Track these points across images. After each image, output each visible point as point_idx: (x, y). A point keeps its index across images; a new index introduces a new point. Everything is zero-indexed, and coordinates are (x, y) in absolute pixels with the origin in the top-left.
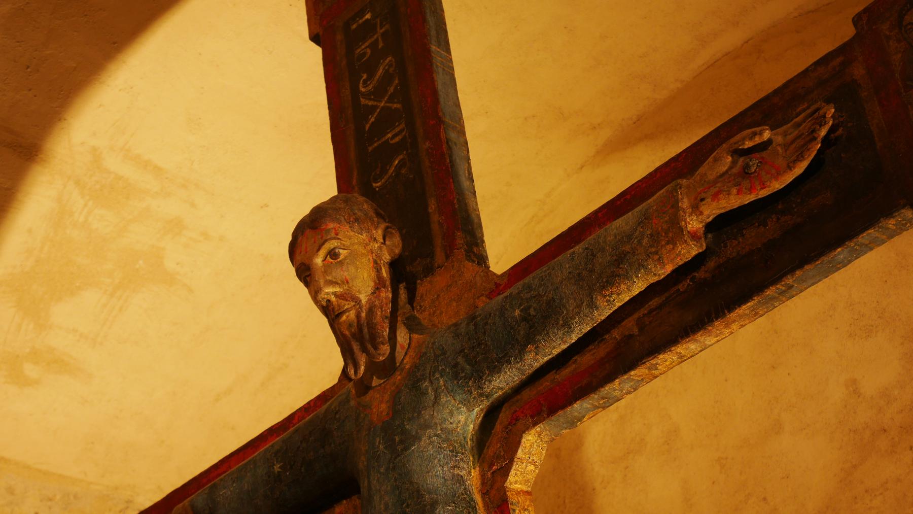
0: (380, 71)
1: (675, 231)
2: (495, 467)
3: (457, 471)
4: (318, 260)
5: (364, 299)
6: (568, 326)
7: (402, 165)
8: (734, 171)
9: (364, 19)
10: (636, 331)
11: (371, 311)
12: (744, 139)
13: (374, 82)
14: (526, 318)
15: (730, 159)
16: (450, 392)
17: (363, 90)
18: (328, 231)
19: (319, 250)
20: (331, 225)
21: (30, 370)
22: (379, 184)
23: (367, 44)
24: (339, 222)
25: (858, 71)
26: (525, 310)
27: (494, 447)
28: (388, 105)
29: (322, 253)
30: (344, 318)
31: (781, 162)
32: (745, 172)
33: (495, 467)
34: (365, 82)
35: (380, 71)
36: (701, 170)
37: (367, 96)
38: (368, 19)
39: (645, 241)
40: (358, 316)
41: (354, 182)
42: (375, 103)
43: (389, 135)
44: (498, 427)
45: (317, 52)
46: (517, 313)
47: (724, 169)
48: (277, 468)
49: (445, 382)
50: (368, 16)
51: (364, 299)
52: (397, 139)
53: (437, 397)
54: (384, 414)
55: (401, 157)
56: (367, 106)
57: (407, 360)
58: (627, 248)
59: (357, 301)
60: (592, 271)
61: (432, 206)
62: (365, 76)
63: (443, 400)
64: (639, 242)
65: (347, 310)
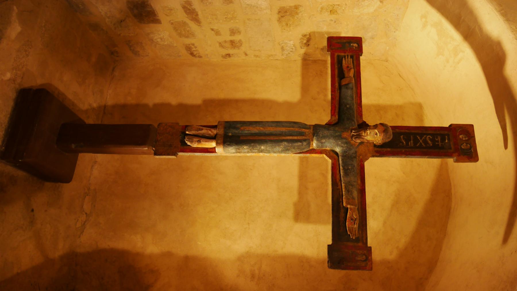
0: (430, 142)
1: (348, 203)
2: (328, 153)
3: (328, 147)
4: (376, 131)
5: (366, 138)
6: (343, 177)
7: (403, 143)
8: (353, 217)
9: (446, 139)
10: (338, 188)
11: (363, 138)
12: (357, 222)
13: (428, 140)
14: (348, 169)
15: (355, 217)
16: (342, 150)
17: (428, 137)
18: (381, 134)
19: (378, 131)
20: (382, 135)
21: (424, 20)
22: (402, 137)
23: (439, 140)
24: (383, 137)
25: (360, 244)
26: (349, 169)
27: (332, 153)
28: (420, 143)
29: (377, 132)
30: (363, 133)
31: (350, 226)
32: (352, 219)
33: (328, 153)
34: (430, 137)
35: (430, 142)
36: (357, 212)
37: (426, 137)
38: (446, 140)
39: (349, 197)
40: (363, 136)
41: (406, 131)
42: (422, 139)
43: (412, 142)
44: (335, 155)
45: (447, 125)
46: (350, 168)
47: (354, 216)
48: (348, 106)
49: (344, 149)
50: (447, 141)
51: (366, 138)
52: (410, 144)
53: (342, 147)
54: (343, 136)
55: (405, 144)
56: (423, 137)
57: (353, 141)
58: (350, 193)
59: (365, 136)
60: (349, 185)
61: (389, 149)
62: (431, 138)
63: (341, 148)
64: (349, 196)
65: (365, 134)
